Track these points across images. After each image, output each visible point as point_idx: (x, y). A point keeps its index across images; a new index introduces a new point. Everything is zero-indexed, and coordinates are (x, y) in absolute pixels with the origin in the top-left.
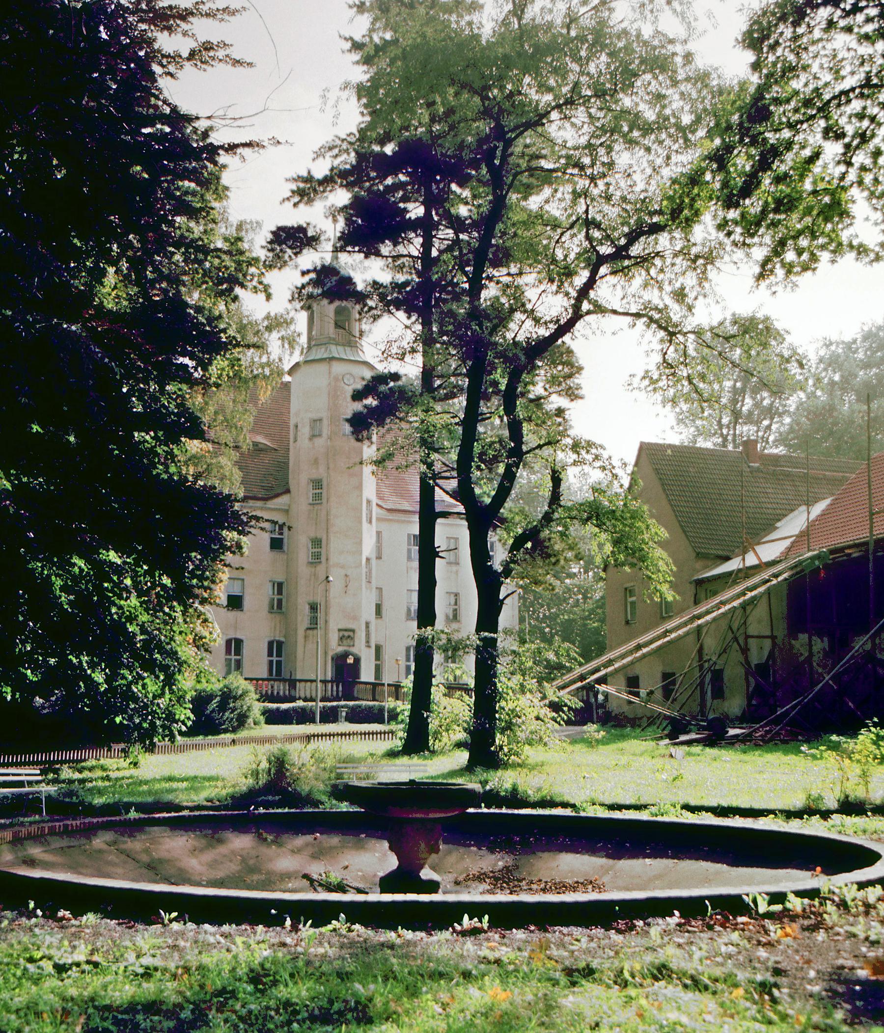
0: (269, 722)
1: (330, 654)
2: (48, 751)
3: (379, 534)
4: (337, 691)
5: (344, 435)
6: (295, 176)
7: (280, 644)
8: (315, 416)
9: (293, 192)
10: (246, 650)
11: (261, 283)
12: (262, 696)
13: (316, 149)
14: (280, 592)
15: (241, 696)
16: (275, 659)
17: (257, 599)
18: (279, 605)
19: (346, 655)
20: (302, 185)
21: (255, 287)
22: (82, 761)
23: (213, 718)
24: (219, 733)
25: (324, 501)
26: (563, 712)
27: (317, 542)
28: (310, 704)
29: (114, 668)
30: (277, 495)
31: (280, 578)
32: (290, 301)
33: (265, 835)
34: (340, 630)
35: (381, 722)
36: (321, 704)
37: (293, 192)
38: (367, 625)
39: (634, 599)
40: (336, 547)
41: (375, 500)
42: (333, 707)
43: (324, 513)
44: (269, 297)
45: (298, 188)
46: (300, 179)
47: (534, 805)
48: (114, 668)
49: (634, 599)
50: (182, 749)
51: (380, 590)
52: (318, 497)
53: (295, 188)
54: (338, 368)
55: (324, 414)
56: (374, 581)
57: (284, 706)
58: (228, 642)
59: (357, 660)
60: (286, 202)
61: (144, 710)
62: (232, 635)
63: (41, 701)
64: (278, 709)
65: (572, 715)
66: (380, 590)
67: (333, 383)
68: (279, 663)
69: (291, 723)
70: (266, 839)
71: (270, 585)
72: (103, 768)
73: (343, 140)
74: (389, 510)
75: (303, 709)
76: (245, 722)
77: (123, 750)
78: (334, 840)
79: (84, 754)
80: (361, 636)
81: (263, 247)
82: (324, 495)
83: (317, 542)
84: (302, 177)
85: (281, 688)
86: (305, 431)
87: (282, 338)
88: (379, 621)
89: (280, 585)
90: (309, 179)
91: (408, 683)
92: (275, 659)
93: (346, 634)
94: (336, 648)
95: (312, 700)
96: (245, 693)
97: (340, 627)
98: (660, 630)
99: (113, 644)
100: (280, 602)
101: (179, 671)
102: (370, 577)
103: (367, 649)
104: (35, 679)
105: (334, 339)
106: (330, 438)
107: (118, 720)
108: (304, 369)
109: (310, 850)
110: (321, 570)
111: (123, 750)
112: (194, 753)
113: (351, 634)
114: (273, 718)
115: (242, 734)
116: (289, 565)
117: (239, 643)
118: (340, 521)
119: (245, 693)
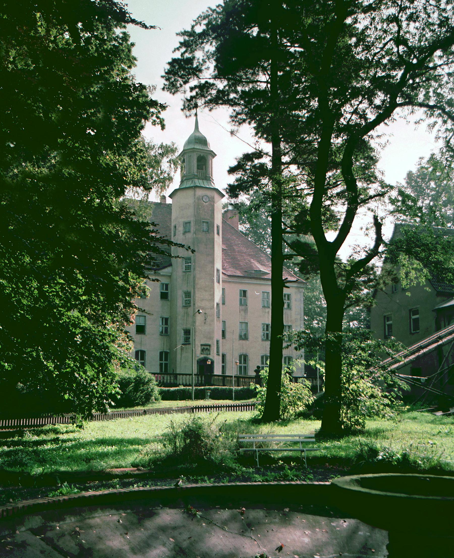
0: (163, 399)
1: (197, 359)
2: (19, 418)
3: (223, 289)
4: (201, 380)
5: (203, 231)
6: (183, 31)
7: (166, 353)
8: (186, 220)
9: (181, 43)
10: (147, 357)
11: (158, 118)
12: (160, 382)
13: (195, 19)
14: (166, 323)
15: (147, 382)
16: (164, 362)
17: (154, 327)
18: (166, 332)
19: (206, 359)
20: (187, 38)
21: (155, 121)
22: (42, 426)
23: (132, 397)
24: (133, 406)
25: (192, 270)
26: (394, 391)
27: (188, 294)
28: (188, 388)
29: (60, 360)
30: (164, 267)
31: (166, 316)
32: (182, 110)
33: (193, 510)
34: (202, 345)
35: (231, 399)
36: (194, 388)
37: (181, 43)
38: (218, 342)
39: (390, 322)
40: (199, 297)
41: (221, 271)
42: (201, 389)
43: (192, 276)
44: (163, 127)
45: (185, 40)
46: (185, 33)
47: (420, 472)
48: (60, 360)
49: (390, 322)
50: (113, 417)
51: (224, 322)
52: (188, 268)
53: (182, 41)
54: (199, 192)
55: (192, 219)
56: (221, 317)
57: (172, 389)
58: (137, 353)
59: (212, 362)
60: (177, 51)
61: (82, 389)
62: (139, 348)
63: (22, 385)
64: (168, 391)
65: (400, 394)
66: (224, 322)
67: (196, 201)
68: (166, 365)
69: (176, 400)
70: (195, 515)
71: (160, 319)
72: (56, 432)
73: (213, 11)
74: (229, 276)
75: (183, 391)
76: (149, 399)
77: (72, 418)
78: (257, 514)
79: (44, 421)
80: (214, 349)
81: (162, 77)
82: (192, 267)
83: (188, 294)
84: (188, 32)
85: (167, 379)
86: (181, 229)
87: (170, 162)
88: (224, 340)
89: (167, 320)
90: (191, 34)
91: (264, 373)
92: (164, 362)
93: (205, 347)
94: (199, 355)
95: (190, 385)
96: (150, 380)
97: (202, 343)
98: (435, 336)
99: (60, 340)
100: (166, 329)
101: (109, 361)
102: (219, 315)
103: (218, 356)
104: (9, 369)
105: (197, 176)
106: (195, 233)
107: (66, 397)
108: (179, 194)
109: (235, 526)
110: (190, 310)
111: (72, 418)
112: (120, 420)
113: (208, 347)
114: (166, 396)
115: (148, 407)
116: (172, 308)
117: (143, 353)
118: (201, 282)
119: (150, 380)
